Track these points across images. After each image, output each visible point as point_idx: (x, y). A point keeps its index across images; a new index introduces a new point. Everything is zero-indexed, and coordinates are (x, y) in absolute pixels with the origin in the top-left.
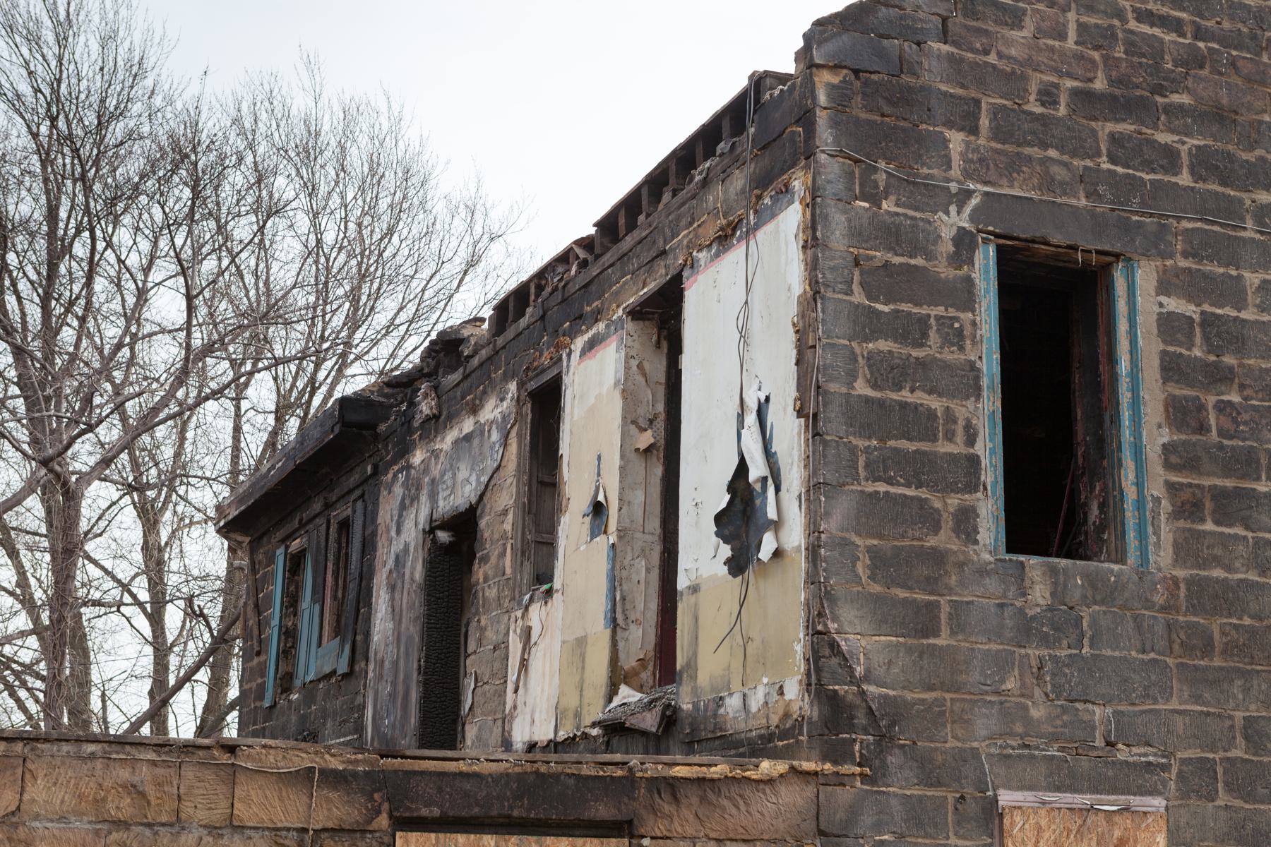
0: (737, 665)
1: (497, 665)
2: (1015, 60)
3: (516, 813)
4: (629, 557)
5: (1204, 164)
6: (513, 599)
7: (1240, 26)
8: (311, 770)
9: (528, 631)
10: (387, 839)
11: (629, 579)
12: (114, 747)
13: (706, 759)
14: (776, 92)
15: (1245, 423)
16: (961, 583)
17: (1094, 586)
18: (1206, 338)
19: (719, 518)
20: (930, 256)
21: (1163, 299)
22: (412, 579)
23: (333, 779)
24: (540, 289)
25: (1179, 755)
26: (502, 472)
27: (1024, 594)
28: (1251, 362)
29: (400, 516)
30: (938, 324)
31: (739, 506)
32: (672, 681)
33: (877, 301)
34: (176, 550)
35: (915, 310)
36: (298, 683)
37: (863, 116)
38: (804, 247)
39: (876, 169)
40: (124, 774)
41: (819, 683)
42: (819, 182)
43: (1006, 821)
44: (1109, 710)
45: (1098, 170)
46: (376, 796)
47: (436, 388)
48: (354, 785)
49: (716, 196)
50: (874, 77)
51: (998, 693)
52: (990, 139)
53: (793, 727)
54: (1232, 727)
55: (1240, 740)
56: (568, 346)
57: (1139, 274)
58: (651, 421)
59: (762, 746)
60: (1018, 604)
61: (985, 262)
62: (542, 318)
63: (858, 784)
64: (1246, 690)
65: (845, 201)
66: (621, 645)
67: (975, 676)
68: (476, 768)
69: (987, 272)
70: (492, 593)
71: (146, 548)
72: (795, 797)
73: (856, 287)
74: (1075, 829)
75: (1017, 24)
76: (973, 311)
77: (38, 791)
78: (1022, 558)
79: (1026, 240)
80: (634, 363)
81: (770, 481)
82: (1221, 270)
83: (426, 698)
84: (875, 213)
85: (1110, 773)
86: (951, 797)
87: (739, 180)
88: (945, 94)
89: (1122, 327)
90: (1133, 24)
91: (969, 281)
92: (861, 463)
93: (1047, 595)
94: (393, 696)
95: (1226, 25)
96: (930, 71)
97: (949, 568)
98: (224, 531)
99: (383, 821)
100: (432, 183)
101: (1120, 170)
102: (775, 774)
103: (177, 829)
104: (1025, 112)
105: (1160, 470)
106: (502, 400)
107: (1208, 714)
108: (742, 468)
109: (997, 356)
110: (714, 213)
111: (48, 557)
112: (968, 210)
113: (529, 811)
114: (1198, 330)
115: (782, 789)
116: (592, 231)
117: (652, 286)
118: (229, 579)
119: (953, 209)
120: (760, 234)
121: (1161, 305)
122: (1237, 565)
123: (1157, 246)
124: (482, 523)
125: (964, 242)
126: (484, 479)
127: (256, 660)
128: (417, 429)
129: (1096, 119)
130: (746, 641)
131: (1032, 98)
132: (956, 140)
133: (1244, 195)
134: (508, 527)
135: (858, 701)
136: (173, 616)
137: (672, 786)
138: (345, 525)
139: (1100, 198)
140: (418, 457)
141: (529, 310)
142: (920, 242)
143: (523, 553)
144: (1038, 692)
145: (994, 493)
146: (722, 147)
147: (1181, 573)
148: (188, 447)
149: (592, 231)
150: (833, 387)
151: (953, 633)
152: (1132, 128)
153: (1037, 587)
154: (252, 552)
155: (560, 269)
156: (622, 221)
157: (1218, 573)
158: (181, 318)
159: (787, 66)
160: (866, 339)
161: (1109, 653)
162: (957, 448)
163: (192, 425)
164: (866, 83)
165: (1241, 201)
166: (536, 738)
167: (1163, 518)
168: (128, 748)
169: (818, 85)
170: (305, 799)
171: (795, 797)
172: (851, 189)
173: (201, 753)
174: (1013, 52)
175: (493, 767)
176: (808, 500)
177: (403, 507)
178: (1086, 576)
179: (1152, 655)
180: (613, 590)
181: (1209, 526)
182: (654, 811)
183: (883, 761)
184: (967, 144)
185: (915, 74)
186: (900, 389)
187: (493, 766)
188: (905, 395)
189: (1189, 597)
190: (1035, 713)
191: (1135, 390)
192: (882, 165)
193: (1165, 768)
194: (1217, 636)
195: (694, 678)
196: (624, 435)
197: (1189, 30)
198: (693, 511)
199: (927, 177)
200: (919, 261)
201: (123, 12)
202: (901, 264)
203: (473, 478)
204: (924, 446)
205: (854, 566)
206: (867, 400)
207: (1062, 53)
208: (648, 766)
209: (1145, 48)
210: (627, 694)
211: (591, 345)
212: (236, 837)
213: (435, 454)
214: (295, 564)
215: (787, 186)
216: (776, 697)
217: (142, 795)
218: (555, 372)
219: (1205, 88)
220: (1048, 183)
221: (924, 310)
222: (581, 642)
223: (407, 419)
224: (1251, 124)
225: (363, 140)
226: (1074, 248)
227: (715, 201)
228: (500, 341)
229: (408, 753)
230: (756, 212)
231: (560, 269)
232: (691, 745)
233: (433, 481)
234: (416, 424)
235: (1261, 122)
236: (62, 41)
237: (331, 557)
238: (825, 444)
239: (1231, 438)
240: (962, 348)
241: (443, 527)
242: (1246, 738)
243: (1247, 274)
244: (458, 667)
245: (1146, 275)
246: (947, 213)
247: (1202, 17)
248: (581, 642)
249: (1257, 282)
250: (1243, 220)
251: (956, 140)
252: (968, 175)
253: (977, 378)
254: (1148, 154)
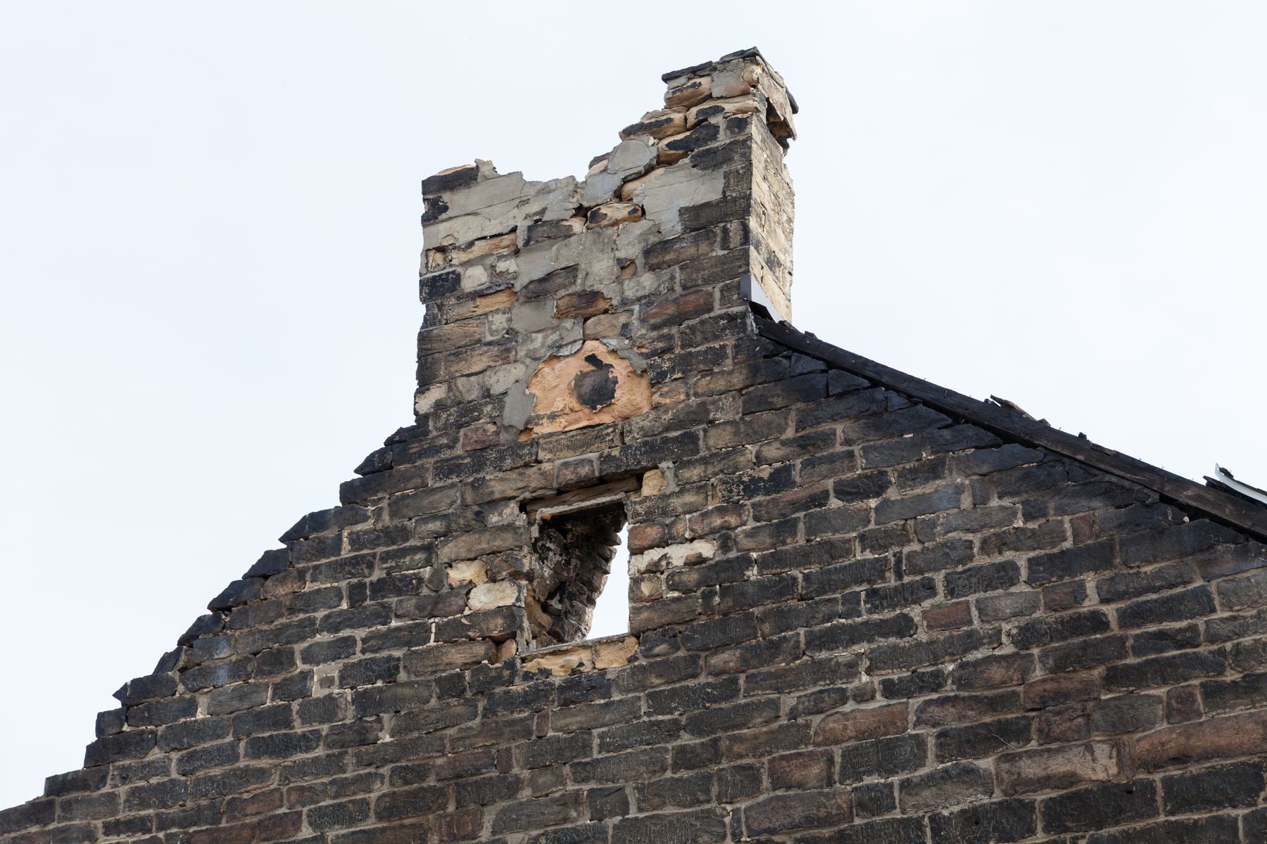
247: (165, 806)
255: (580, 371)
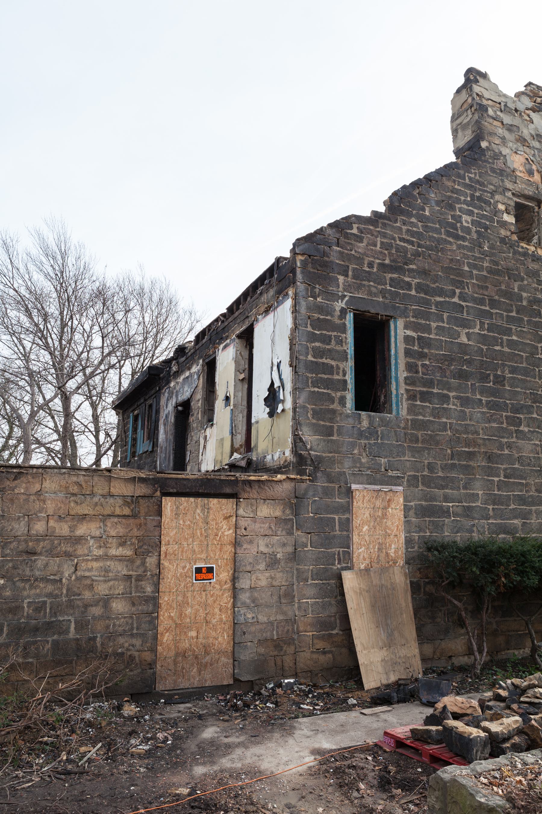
0: (270, 446)
1: (197, 447)
2: (360, 253)
3: (200, 491)
4: (237, 413)
5: (420, 288)
6: (201, 427)
7: (432, 243)
8: (135, 477)
9: (206, 437)
10: (159, 499)
11: (237, 420)
12: (71, 470)
13: (260, 474)
14: (284, 263)
15: (430, 371)
16: (341, 420)
17: (382, 421)
18: (419, 344)
19: (265, 400)
20: (332, 316)
21: (405, 331)
22: (171, 422)
23: (142, 480)
24: (209, 330)
25: (407, 474)
26: (198, 388)
27: (360, 424)
28: (433, 351)
29: (167, 402)
30: (335, 338)
31: (271, 396)
32: (250, 451)
33: (315, 330)
34: (102, 415)
35: (327, 333)
36: (137, 454)
37: (312, 270)
38: (292, 313)
39: (315, 288)
40: (75, 479)
41: (296, 451)
42: (297, 291)
43: (354, 494)
44: (386, 460)
45: (386, 289)
46: (156, 486)
47: (177, 363)
48: (149, 482)
49: (264, 298)
50: (315, 258)
51: (352, 454)
52: (352, 279)
53: (288, 464)
54: (424, 465)
55: (426, 469)
56: (218, 347)
57: (398, 323)
58: (244, 371)
59: (278, 470)
60: (358, 426)
61: (349, 319)
62: (210, 339)
63: (308, 482)
64: (428, 454)
65: (306, 298)
66: (234, 440)
67: (345, 449)
68: (187, 477)
69: (350, 322)
70: (195, 425)
71: (93, 416)
72: (288, 486)
73: (309, 326)
74: (375, 496)
75: (361, 241)
76: (346, 334)
77: (47, 484)
78: (360, 412)
79: (363, 311)
80: (238, 352)
81: (281, 387)
82: (424, 322)
83: (175, 458)
84: (315, 302)
85: (386, 479)
86: (337, 486)
87: (272, 292)
88: (338, 264)
89: (393, 339)
90: (398, 242)
91: (344, 324)
92: (310, 382)
93: (368, 424)
94: (165, 457)
95: (428, 243)
96: (333, 256)
97: (337, 415)
98: (113, 409)
99: (158, 493)
100: (178, 304)
101: (393, 289)
102: (282, 479)
103: (92, 496)
104: (363, 270)
105: (404, 385)
106: (198, 365)
107: (417, 461)
108: (272, 384)
109: (353, 348)
110: (264, 303)
111: (63, 419)
112: (344, 301)
113: (204, 490)
114: (416, 341)
115: (284, 484)
116: (225, 311)
117: (244, 327)
118: (118, 423)
119: (340, 301)
120: (278, 309)
121: (405, 333)
122: (427, 415)
123: (404, 314)
124: (192, 404)
125: (343, 312)
126: (192, 390)
127: (125, 448)
128: (172, 375)
129: (385, 273)
130: (273, 438)
131: (365, 266)
132: (341, 279)
133: (432, 298)
134: (200, 405)
135: (308, 457)
136: (102, 436)
137: (250, 483)
138: (151, 406)
139: (386, 298)
140: (172, 384)
141: (206, 337)
142: (329, 311)
143: (204, 413)
144: (364, 454)
145: (351, 392)
146: (266, 282)
147: (409, 417)
148: (105, 385)
149: (225, 311)
150: (301, 357)
151: (338, 435)
152: (397, 276)
153: (364, 421)
154: (123, 415)
155: (215, 324)
156: (235, 307)
157: (421, 417)
158: (101, 345)
159: (287, 255)
160: (312, 342)
161: (386, 442)
162: (340, 377)
163: (107, 378)
164: (313, 260)
165: (431, 300)
166: (208, 469)
167: (404, 400)
168: (76, 470)
169: (297, 260)
170: (133, 487)
171: (288, 486)
172: (307, 294)
173: (99, 472)
174: (360, 250)
175: (193, 476)
176: (293, 393)
177: (168, 400)
178: (380, 418)
179: (400, 443)
180: (232, 423)
181: (418, 403)
182: (244, 490)
183: (316, 475)
184: (345, 280)
185: (328, 257)
186: (322, 358)
187: (193, 476)
188: (324, 360)
189: (411, 425)
190: (363, 460)
191: (396, 359)
192: (317, 286)
193: (403, 478)
194: (420, 437)
195: (257, 450)
196: (235, 375)
197: (416, 244)
198: (257, 398)
199: (332, 290)
200: (329, 318)
201: (82, 250)
202: (323, 319)
203: (189, 390)
204: (330, 376)
205: (307, 414)
206: (312, 361)
207: (375, 251)
208: (243, 476)
209: (402, 250)
210: (236, 456)
211: (225, 347)
212: (111, 499)
213: (177, 383)
214: (136, 418)
215: (287, 293)
216: (282, 455)
217: (81, 485)
218: (214, 356)
219: (420, 264)
220: (370, 293)
221: (330, 333)
222: (222, 440)
223: (169, 372)
224: (435, 275)
225: (158, 291)
226: (378, 314)
227: (264, 299)
228: (197, 347)
229: (166, 472)
230: (277, 302)
231: (215, 324)
232: (256, 470)
233: (177, 391)
234: (171, 374)
235: (438, 275)
236: (63, 258)
237: (146, 416)
238: (299, 375)
239: (426, 375)
240: (342, 346)
241: (180, 406)
242: (428, 469)
243: (432, 324)
244: (185, 448)
245: (400, 323)
246: (338, 302)
247: (420, 240)
248: (222, 440)
249: (435, 326)
250: (431, 306)
251: (341, 279)
252: (345, 290)
253: (347, 355)
254: (402, 284)
255: (316, 752)
